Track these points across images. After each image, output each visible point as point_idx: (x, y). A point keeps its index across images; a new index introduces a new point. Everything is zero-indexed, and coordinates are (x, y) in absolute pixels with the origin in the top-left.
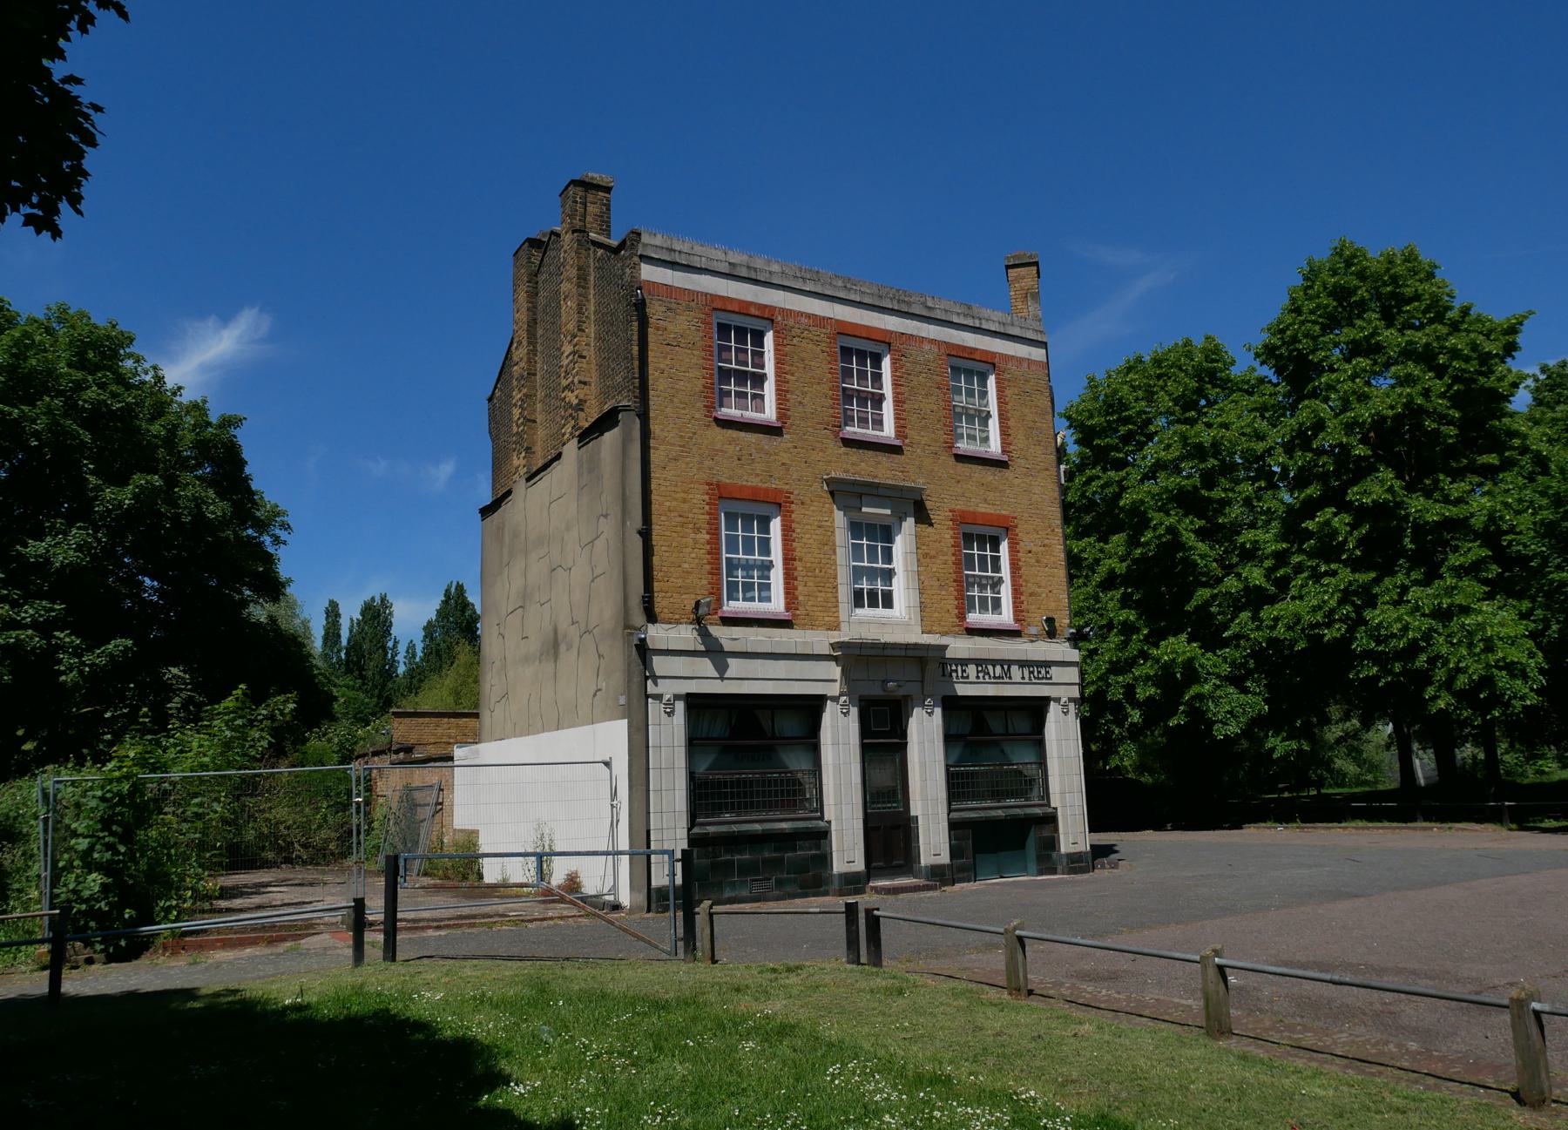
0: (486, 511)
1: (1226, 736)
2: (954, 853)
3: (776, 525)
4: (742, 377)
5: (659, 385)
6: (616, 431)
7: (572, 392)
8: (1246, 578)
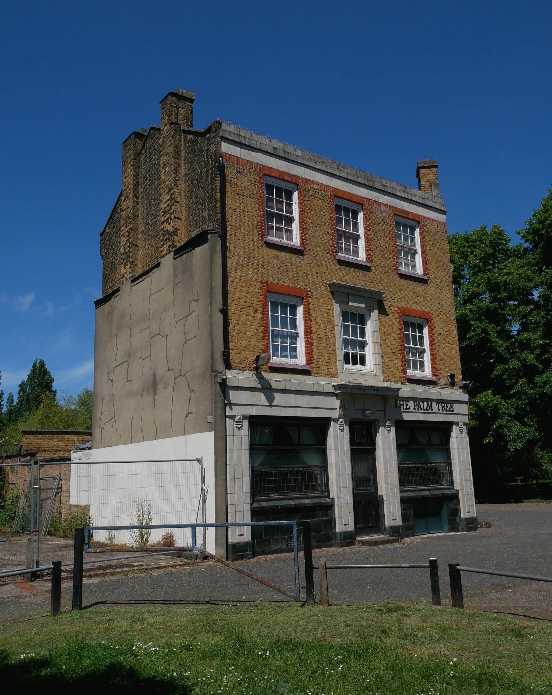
0: (99, 303)
1: (516, 449)
2: (405, 518)
3: (300, 311)
4: (280, 218)
5: (232, 218)
6: (205, 246)
7: (169, 224)
8: (525, 360)
